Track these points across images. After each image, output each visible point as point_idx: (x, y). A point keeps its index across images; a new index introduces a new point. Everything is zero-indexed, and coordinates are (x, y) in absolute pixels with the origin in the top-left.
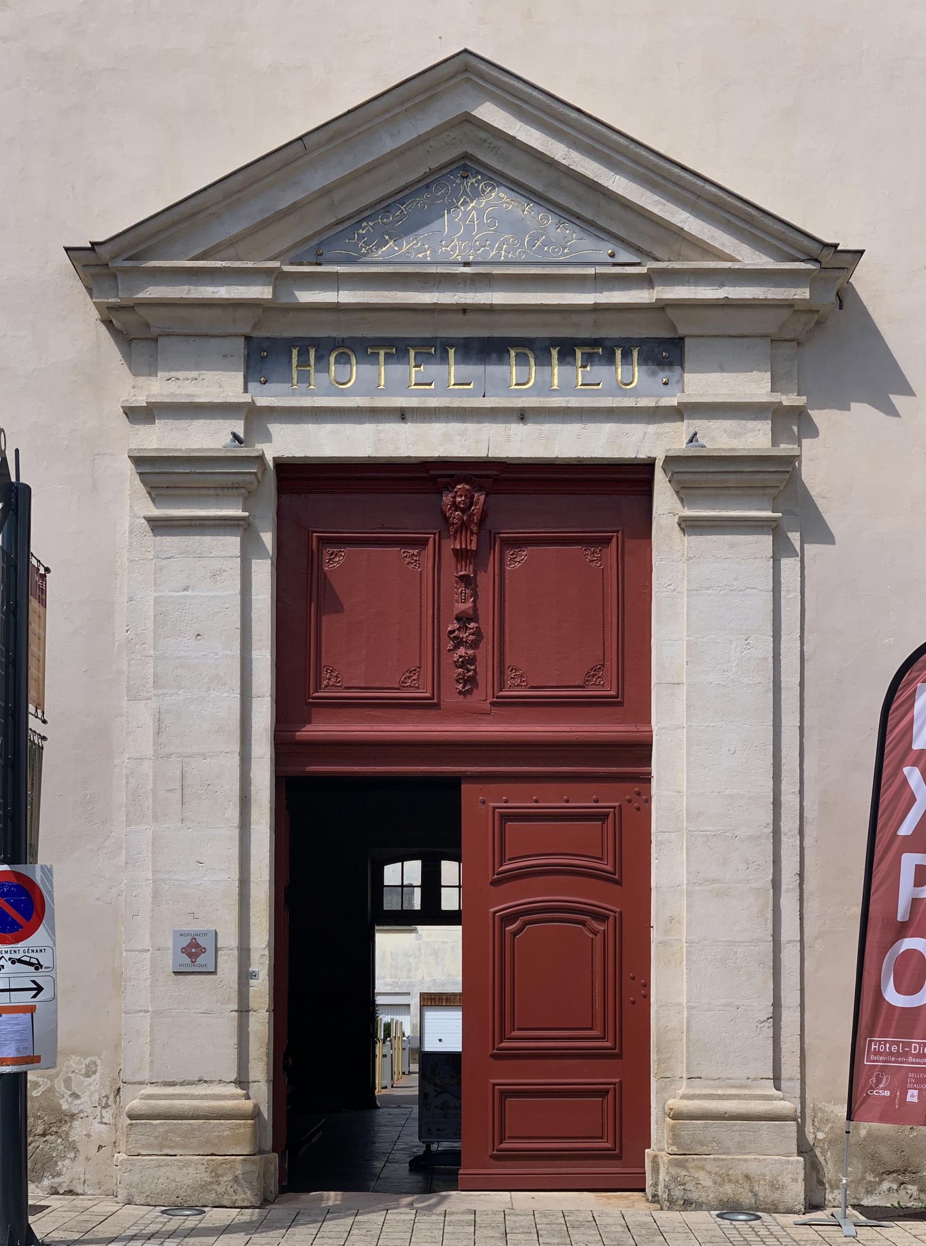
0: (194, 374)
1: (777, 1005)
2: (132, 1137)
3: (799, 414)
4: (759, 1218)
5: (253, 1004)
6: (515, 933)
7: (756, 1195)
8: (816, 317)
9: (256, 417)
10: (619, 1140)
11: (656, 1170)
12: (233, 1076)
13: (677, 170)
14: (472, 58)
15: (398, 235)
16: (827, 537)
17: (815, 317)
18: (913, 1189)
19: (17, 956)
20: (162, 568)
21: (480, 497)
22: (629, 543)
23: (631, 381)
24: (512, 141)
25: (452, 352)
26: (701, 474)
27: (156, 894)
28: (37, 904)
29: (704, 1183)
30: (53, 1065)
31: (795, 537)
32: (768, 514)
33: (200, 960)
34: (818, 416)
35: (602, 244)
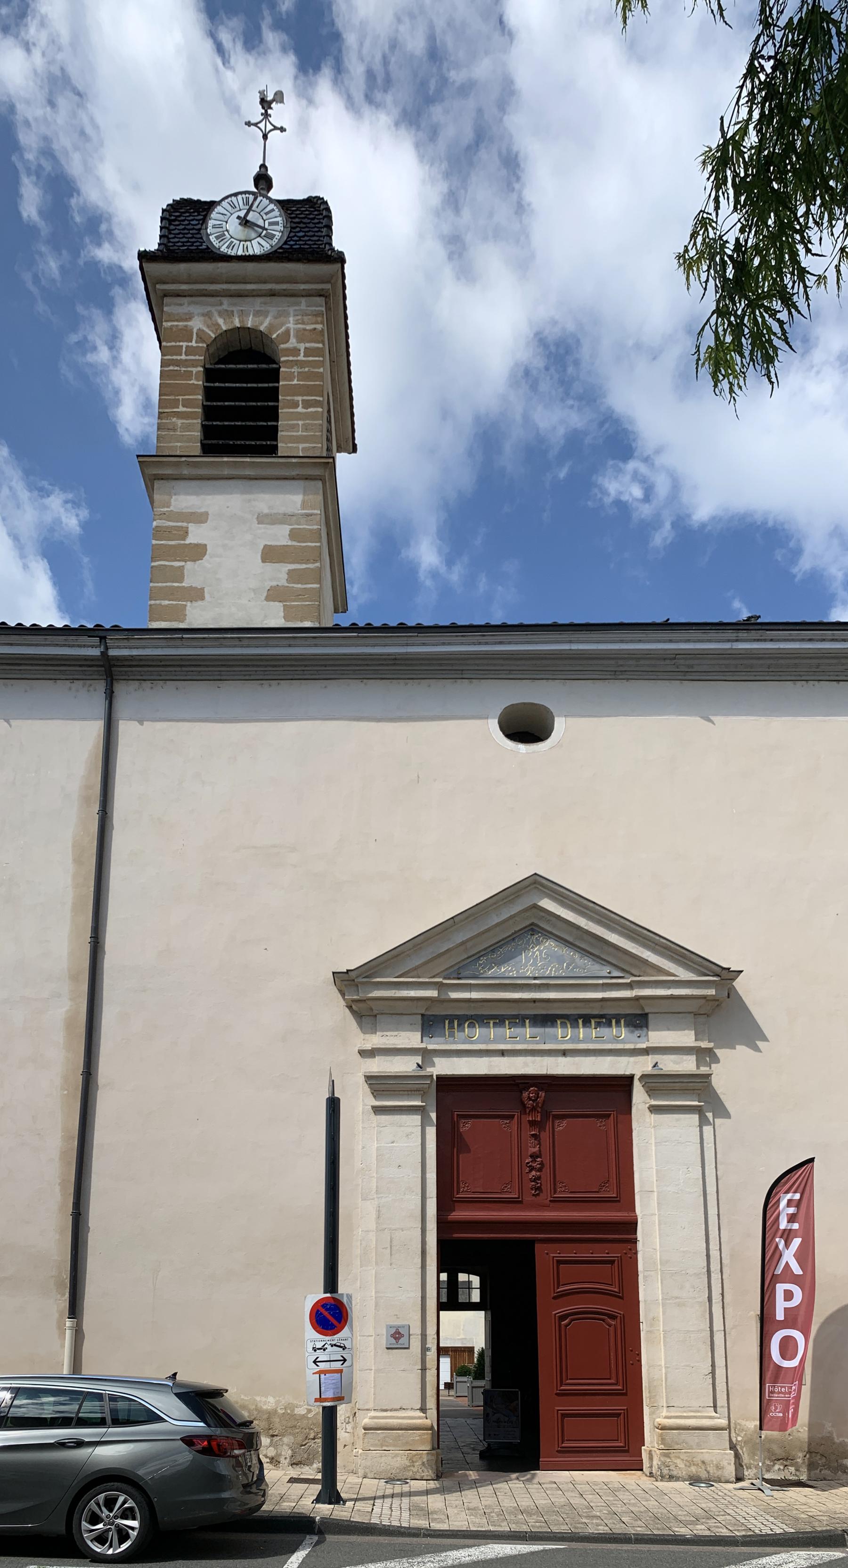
0: (396, 1033)
1: (713, 1365)
2: (366, 1440)
3: (709, 1051)
4: (713, 1486)
5: (428, 1366)
6: (567, 1325)
7: (708, 1472)
8: (717, 1003)
9: (427, 1055)
10: (627, 1442)
11: (651, 1458)
12: (419, 1406)
13: (645, 932)
14: (538, 878)
15: (499, 964)
16: (726, 1114)
17: (717, 1004)
18: (792, 1469)
19: (334, 1343)
20: (380, 1132)
21: (542, 1094)
22: (621, 1117)
23: (623, 1036)
24: (559, 917)
25: (527, 1021)
26: (657, 1083)
27: (377, 1305)
28: (344, 1314)
29: (680, 1466)
30: (350, 1402)
31: (710, 1115)
32: (696, 1103)
33: (401, 1341)
34: (719, 1052)
35: (604, 968)
